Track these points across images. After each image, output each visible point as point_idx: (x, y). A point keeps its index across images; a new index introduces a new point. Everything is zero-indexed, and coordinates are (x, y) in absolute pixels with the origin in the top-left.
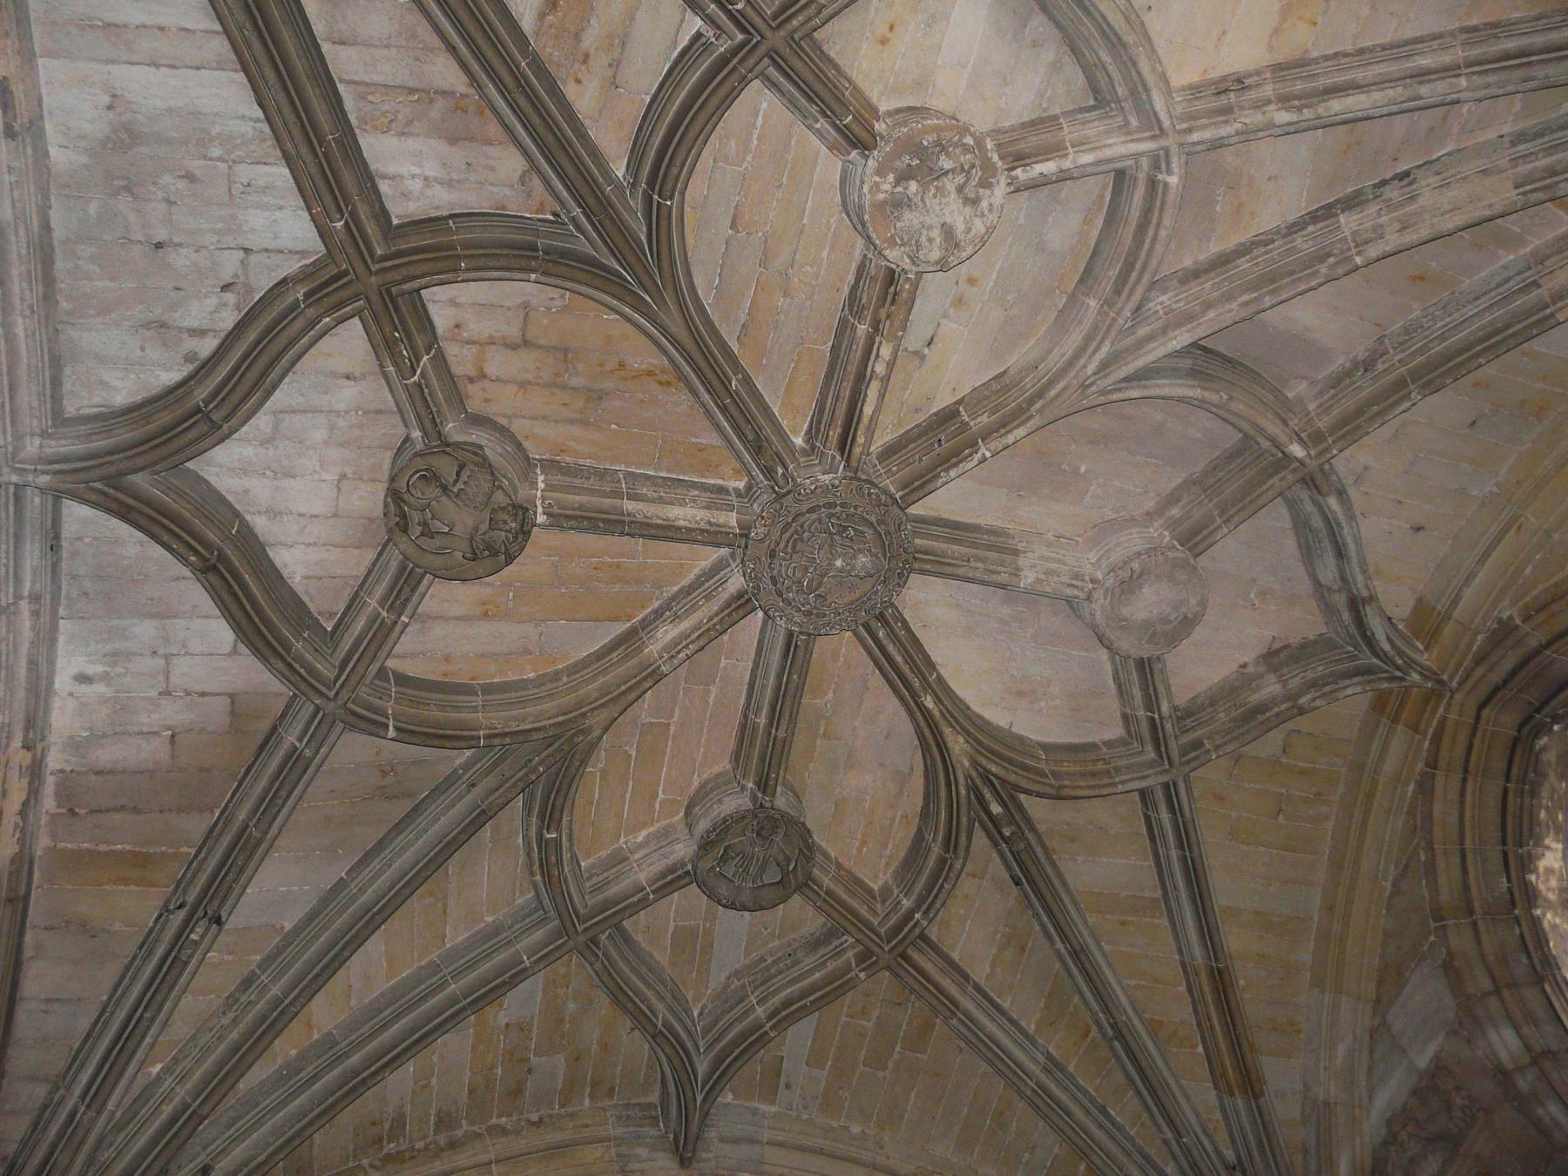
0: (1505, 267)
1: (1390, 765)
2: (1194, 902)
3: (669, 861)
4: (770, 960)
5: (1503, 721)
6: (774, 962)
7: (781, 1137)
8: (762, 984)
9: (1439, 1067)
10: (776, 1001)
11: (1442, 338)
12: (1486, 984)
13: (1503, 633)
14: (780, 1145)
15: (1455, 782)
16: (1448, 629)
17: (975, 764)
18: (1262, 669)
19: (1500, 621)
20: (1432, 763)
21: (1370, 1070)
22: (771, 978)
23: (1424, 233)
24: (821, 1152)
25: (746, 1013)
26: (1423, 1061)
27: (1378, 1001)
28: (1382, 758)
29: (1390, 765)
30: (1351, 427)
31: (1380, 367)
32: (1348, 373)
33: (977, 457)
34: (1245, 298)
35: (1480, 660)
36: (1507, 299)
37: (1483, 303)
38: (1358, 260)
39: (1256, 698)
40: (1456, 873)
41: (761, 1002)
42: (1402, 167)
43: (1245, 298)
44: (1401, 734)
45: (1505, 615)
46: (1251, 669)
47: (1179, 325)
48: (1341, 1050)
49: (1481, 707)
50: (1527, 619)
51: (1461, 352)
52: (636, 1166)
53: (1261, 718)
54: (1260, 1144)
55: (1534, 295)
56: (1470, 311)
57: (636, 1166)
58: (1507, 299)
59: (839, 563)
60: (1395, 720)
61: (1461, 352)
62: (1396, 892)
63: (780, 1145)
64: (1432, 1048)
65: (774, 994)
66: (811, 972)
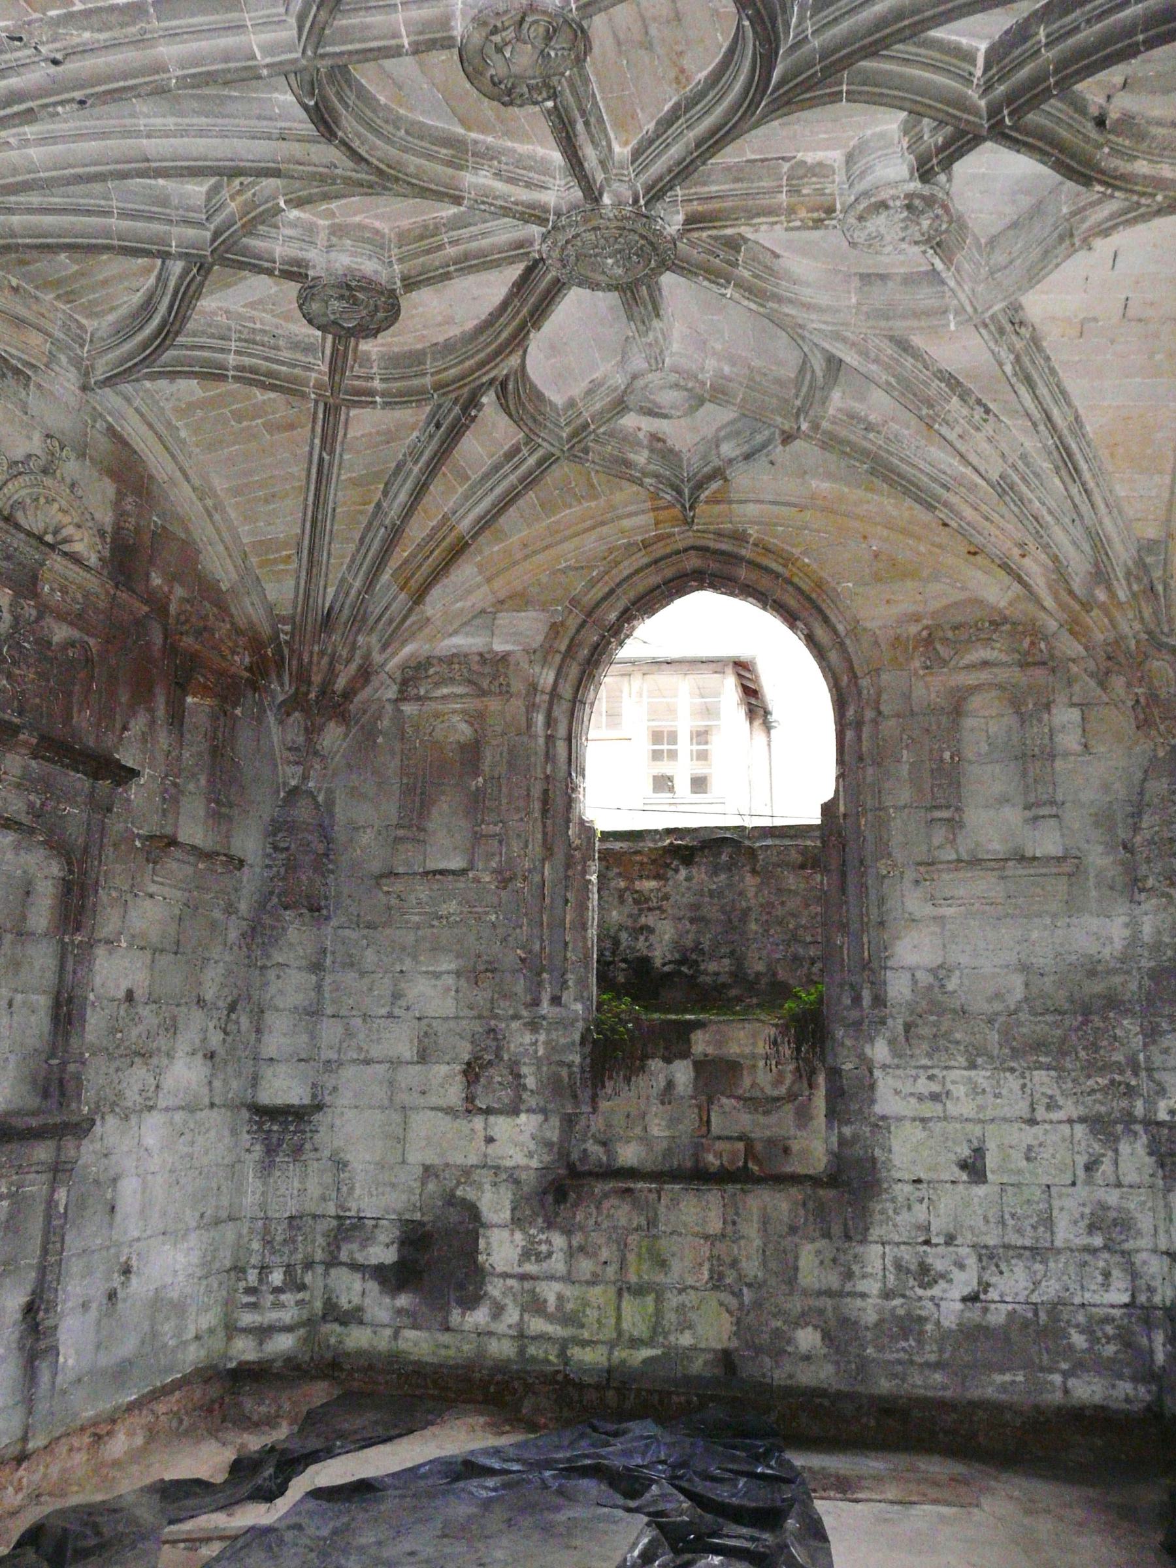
0: (950, 465)
1: (626, 523)
2: (494, 506)
3: (301, 255)
4: (258, 326)
5: (693, 562)
6: (261, 331)
7: (144, 410)
8: (246, 341)
9: (504, 658)
10: (247, 361)
11: (902, 460)
12: (563, 648)
13: (739, 537)
14: (142, 415)
15: (646, 560)
16: (722, 507)
17: (507, 377)
18: (645, 442)
19: (744, 531)
20: (646, 545)
21: (465, 624)
22: (255, 343)
23: (963, 449)
24: (160, 437)
25: (222, 350)
26: (499, 647)
27: (502, 602)
28: (630, 515)
29: (626, 523)
30: (831, 442)
31: (871, 436)
32: (860, 420)
33: (723, 291)
34: (892, 380)
35: (719, 534)
36: (934, 480)
37: (928, 469)
38: (936, 426)
39: (632, 456)
40: (600, 595)
41: (237, 353)
42: (991, 406)
43: (892, 380)
44: (649, 518)
45: (750, 531)
46: (641, 435)
47: (860, 353)
48: (459, 605)
49: (693, 548)
50: (756, 545)
51: (899, 475)
52: (57, 368)
53: (624, 469)
54: (391, 621)
55: (941, 491)
56: (922, 465)
57: (57, 368)
58: (934, 480)
59: (610, 261)
60: (654, 510)
61: (899, 475)
62: (563, 571)
63: (142, 415)
64: (509, 647)
65: (250, 355)
66: (283, 363)
